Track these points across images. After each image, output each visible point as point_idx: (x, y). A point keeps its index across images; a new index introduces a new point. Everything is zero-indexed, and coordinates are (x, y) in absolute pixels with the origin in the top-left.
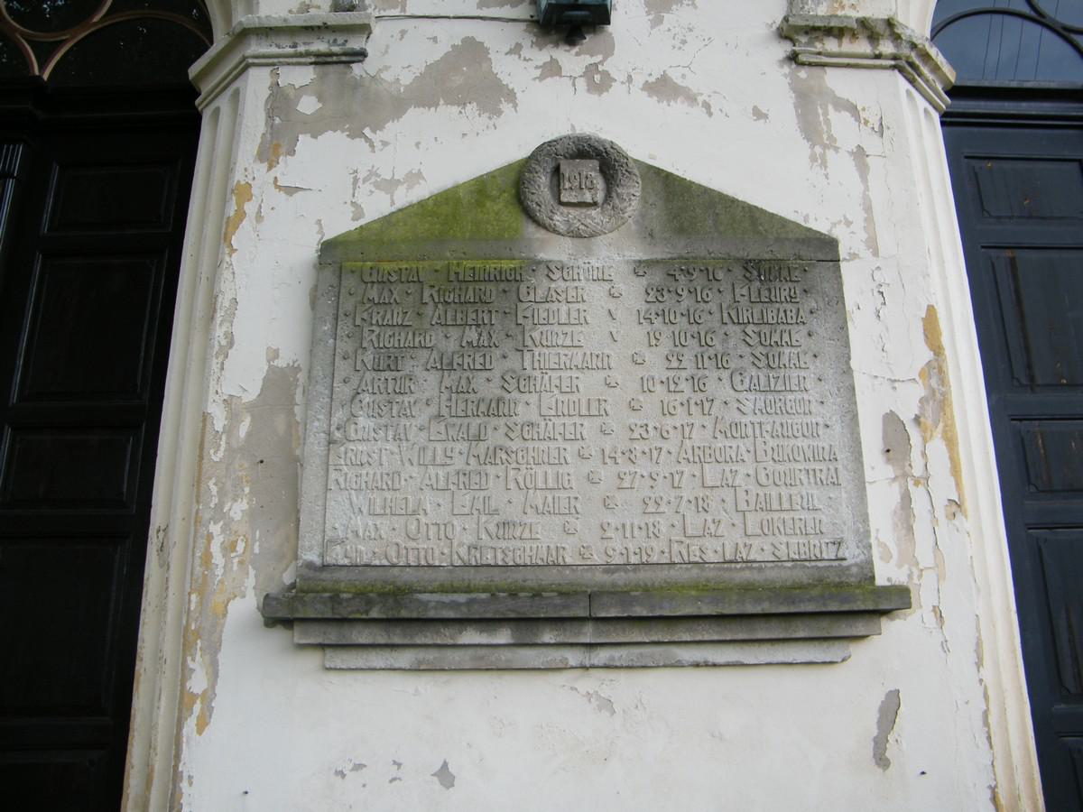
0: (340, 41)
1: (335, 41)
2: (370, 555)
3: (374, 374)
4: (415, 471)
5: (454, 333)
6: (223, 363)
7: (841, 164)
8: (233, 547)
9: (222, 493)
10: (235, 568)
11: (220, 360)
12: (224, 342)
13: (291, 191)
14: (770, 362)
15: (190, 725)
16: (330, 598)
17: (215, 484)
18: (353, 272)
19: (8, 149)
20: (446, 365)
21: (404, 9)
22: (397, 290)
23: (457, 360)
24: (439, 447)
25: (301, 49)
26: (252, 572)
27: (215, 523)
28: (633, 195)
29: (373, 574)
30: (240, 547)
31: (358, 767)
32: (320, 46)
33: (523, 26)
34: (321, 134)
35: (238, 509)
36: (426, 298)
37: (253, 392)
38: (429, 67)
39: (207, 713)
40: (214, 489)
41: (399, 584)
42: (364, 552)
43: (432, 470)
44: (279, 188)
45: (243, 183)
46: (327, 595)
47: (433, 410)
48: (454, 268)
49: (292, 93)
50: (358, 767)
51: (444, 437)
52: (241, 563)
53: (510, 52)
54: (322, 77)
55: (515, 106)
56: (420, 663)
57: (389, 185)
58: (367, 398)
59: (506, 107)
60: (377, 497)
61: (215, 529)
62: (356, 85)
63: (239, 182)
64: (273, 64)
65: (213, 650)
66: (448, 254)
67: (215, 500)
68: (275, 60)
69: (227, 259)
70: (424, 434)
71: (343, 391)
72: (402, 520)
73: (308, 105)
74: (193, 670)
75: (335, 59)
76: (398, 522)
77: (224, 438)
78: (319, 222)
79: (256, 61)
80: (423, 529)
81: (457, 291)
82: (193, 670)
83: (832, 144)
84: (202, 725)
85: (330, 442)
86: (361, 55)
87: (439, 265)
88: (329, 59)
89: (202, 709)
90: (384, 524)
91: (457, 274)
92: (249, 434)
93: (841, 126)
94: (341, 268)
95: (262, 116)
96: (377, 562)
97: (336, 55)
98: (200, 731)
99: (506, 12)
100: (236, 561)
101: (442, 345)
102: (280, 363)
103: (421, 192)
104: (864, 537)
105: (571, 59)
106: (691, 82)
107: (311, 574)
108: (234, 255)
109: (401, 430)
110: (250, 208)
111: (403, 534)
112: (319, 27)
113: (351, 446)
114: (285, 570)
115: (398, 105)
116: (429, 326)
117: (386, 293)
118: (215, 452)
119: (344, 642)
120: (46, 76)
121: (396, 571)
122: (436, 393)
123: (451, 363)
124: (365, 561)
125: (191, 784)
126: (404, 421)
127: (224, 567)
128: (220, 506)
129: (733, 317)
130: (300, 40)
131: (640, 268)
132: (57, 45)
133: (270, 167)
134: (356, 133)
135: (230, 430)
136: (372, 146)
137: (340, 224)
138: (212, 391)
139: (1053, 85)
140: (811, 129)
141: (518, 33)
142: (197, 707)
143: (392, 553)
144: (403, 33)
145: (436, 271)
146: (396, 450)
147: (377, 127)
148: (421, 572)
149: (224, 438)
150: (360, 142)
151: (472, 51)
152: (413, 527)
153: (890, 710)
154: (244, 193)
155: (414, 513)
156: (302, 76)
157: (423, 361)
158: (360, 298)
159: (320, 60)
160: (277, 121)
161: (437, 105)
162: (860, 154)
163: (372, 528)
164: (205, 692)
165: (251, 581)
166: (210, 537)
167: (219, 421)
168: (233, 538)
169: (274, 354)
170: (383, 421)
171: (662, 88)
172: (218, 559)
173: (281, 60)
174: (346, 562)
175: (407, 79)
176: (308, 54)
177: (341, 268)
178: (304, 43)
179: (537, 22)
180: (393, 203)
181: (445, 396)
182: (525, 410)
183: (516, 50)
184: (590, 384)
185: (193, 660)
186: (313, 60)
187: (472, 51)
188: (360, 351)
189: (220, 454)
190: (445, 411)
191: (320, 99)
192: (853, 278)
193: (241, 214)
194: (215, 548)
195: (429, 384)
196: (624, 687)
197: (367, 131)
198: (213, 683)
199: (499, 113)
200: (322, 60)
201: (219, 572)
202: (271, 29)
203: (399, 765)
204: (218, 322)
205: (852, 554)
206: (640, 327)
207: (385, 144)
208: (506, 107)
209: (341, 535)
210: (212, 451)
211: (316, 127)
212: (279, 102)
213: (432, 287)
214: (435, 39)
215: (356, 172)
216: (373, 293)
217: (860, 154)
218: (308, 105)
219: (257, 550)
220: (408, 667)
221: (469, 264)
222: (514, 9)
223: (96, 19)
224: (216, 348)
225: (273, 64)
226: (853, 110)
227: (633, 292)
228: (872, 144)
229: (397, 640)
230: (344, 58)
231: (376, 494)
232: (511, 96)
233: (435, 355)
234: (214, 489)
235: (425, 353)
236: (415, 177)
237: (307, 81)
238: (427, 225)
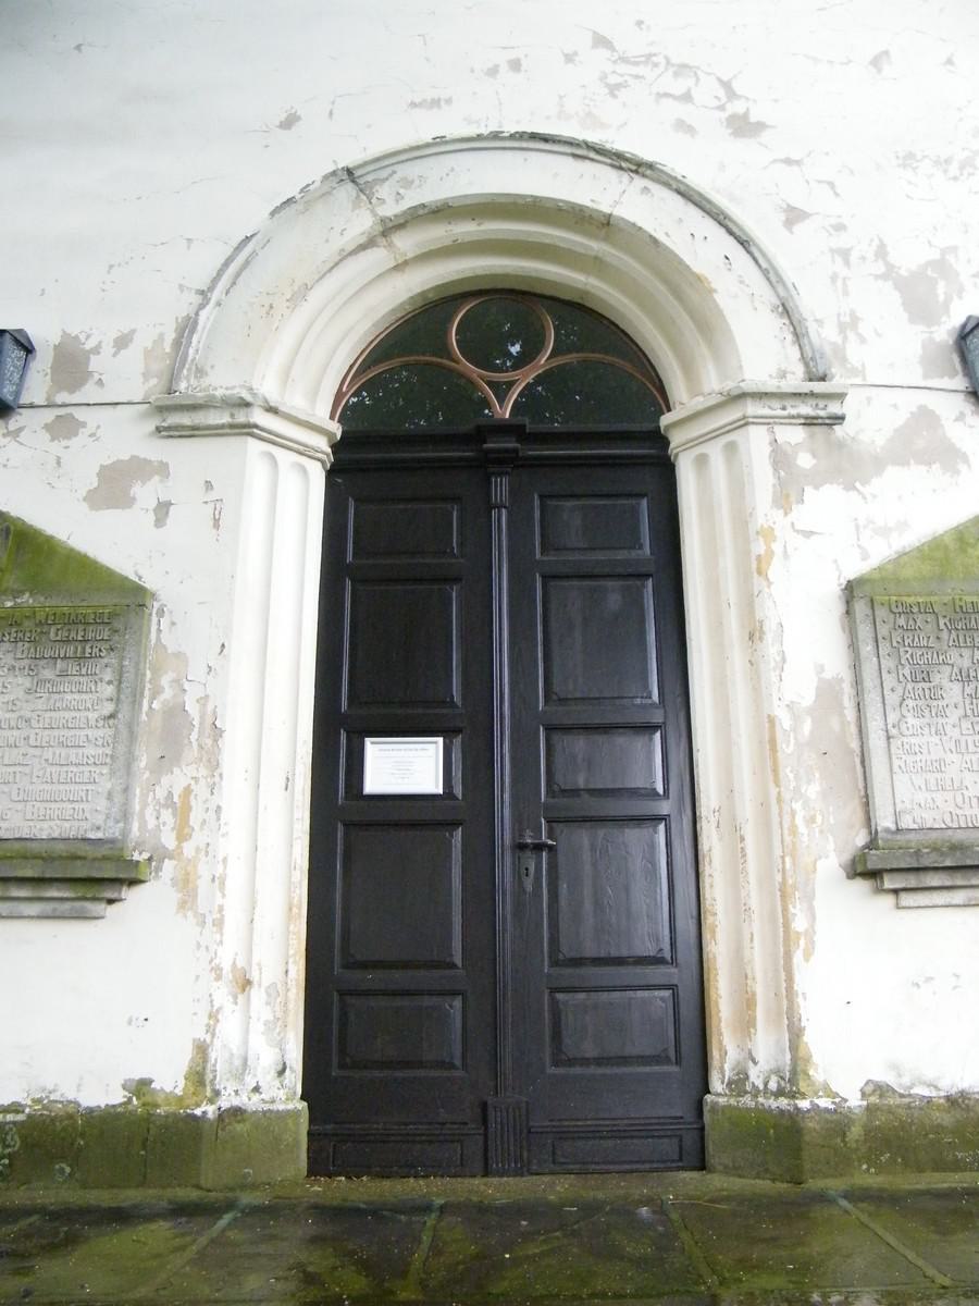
0: (821, 405)
1: (817, 405)
2: (932, 820)
3: (913, 684)
4: (954, 757)
5: (966, 653)
6: (781, 676)
8: (813, 820)
9: (797, 777)
10: (817, 835)
11: (777, 673)
12: (778, 659)
13: (808, 534)
15: (798, 958)
16: (915, 852)
17: (791, 772)
18: (882, 604)
19: (496, 482)
21: (864, 379)
22: (920, 619)
23: (972, 674)
24: (970, 739)
25: (794, 412)
26: (831, 839)
27: (796, 801)
29: (934, 835)
30: (819, 819)
31: (928, 979)
32: (806, 409)
33: (962, 396)
34: (822, 485)
35: (813, 790)
36: (942, 626)
37: (808, 698)
38: (896, 431)
39: (811, 943)
40: (791, 776)
41: (953, 841)
42: (930, 819)
43: (967, 758)
44: (798, 531)
45: (765, 526)
46: (912, 850)
47: (961, 712)
48: (957, 602)
49: (789, 450)
50: (928, 979)
51: (971, 732)
52: (821, 832)
53: (957, 420)
54: (812, 436)
55: (969, 466)
56: (970, 900)
57: (884, 532)
58: (911, 703)
59: (962, 467)
60: (932, 778)
61: (797, 806)
62: (841, 445)
63: (762, 526)
64: (769, 424)
65: (810, 898)
66: (949, 591)
67: (793, 784)
68: (772, 421)
69: (766, 590)
70: (957, 730)
71: (893, 699)
72: (952, 793)
73: (805, 461)
74: (795, 915)
75: (820, 421)
76: (949, 796)
77: (792, 735)
78: (835, 561)
79: (755, 420)
80: (967, 800)
81: (964, 621)
82: (795, 915)
84: (807, 956)
85: (888, 738)
86: (840, 419)
87: (946, 599)
88: (815, 421)
89: (806, 944)
90: (939, 797)
91: (961, 607)
92: (812, 732)
94: (872, 601)
95: (769, 470)
96: (937, 826)
97: (822, 418)
98: (807, 959)
99: (946, 383)
100: (817, 830)
101: (959, 661)
102: (828, 675)
107: (889, 837)
108: (772, 587)
109: (940, 727)
110: (777, 547)
111: (954, 805)
112: (806, 394)
113: (905, 740)
114: (857, 835)
115: (879, 464)
116: (946, 647)
117: (911, 622)
118: (788, 746)
119: (920, 886)
120: (507, 416)
121: (950, 832)
122: (961, 698)
123: (969, 676)
124: (928, 826)
125: (805, 999)
126: (940, 720)
127: (809, 835)
128: (797, 790)
130: (788, 403)
132: (511, 384)
133: (786, 514)
134: (850, 487)
135: (795, 729)
136: (865, 498)
138: (775, 698)
142: (802, 942)
143: (948, 821)
144: (869, 399)
145: (945, 604)
146: (939, 743)
147: (865, 482)
148: (969, 832)
149: (792, 735)
150: (853, 494)
152: (959, 800)
154: (768, 534)
155: (960, 789)
156: (794, 435)
157: (947, 674)
158: (892, 626)
159: (808, 421)
160: (782, 473)
161: (908, 464)
163: (930, 800)
164: (807, 931)
165: (831, 846)
166: (793, 813)
167: (785, 720)
168: (812, 813)
169: (821, 669)
170: (926, 720)
172: (802, 829)
173: (777, 420)
174: (916, 826)
175: (880, 441)
176: (799, 416)
177: (872, 601)
178: (792, 406)
179: (969, 393)
180: (890, 547)
181: (968, 701)
183: (961, 417)
185: (794, 907)
186: (803, 421)
188: (900, 667)
189: (791, 748)
190: (969, 712)
191: (814, 456)
193: (770, 553)
194: (799, 821)
197: (858, 485)
198: (813, 917)
199: (958, 472)
200: (810, 422)
201: (805, 839)
202: (766, 394)
203: (958, 976)
204: (770, 642)
206: (23, 436)
207: (874, 496)
208: (962, 467)
209: (909, 806)
210: (784, 746)
211: (818, 479)
212: (780, 458)
213: (945, 617)
214: (895, 406)
215: (856, 519)
216: (902, 621)
218: (805, 461)
219: (832, 821)
220: (961, 903)
221: (969, 599)
222: (954, 381)
223: (542, 362)
224: (773, 664)
225: (769, 424)
229: (959, 882)
230: (827, 421)
231: (929, 775)
232: (965, 459)
233: (956, 670)
234: (791, 776)
235: (949, 668)
236: (903, 526)
237: (801, 440)
238: (929, 567)
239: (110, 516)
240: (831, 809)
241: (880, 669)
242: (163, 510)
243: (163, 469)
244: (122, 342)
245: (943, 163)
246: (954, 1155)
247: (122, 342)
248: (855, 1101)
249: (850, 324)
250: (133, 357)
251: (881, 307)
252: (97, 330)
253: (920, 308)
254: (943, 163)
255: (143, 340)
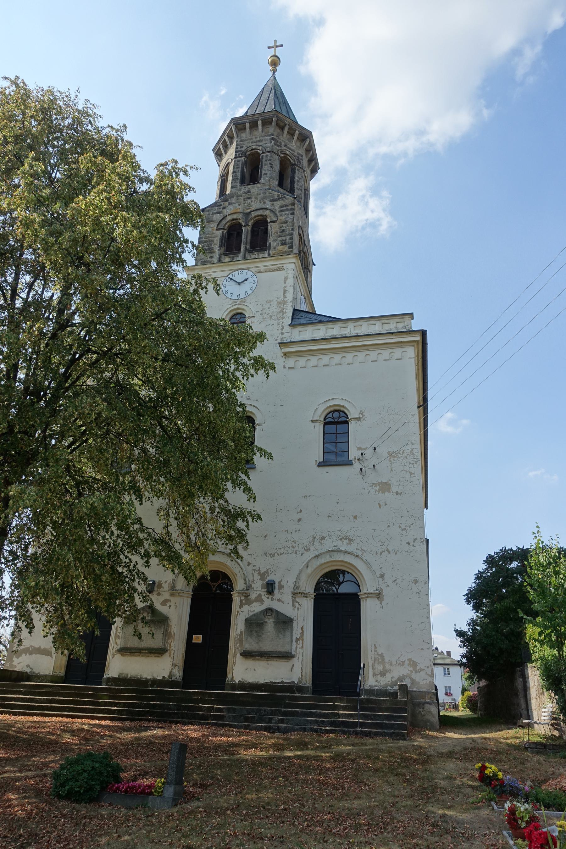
7: (296, 609)
14: (284, 633)
20: (256, 632)
28: (274, 614)
83: (295, 607)
93: (297, 604)
103: (254, 613)
104: (291, 650)
105: (270, 597)
106: (282, 600)
129: (326, 320)
131: (274, 622)
137: (247, 616)
139: (261, 680)
140: (294, 606)
141: (265, 593)
151: (260, 595)
153: (293, 666)
162: (298, 608)
171: (279, 600)
182: (263, 636)
184: (269, 634)
187: (260, 595)
192: (295, 625)
195: (255, 634)
196: (270, 662)
205: (290, 651)
217: (298, 608)
218: (244, 602)
226: (298, 603)
227: (273, 625)
228: (300, 607)
236: (254, 611)
239: (164, 607)
240: (238, 645)
241: (268, 100)
242: (170, 606)
243: (170, 601)
244: (166, 582)
245: (270, 554)
246: (58, 143)
247: (166, 582)
248: (237, 682)
249: (253, 581)
250: (167, 584)
251: (257, 577)
252: (164, 580)
253: (262, 579)
254: (270, 554)
255: (168, 582)
